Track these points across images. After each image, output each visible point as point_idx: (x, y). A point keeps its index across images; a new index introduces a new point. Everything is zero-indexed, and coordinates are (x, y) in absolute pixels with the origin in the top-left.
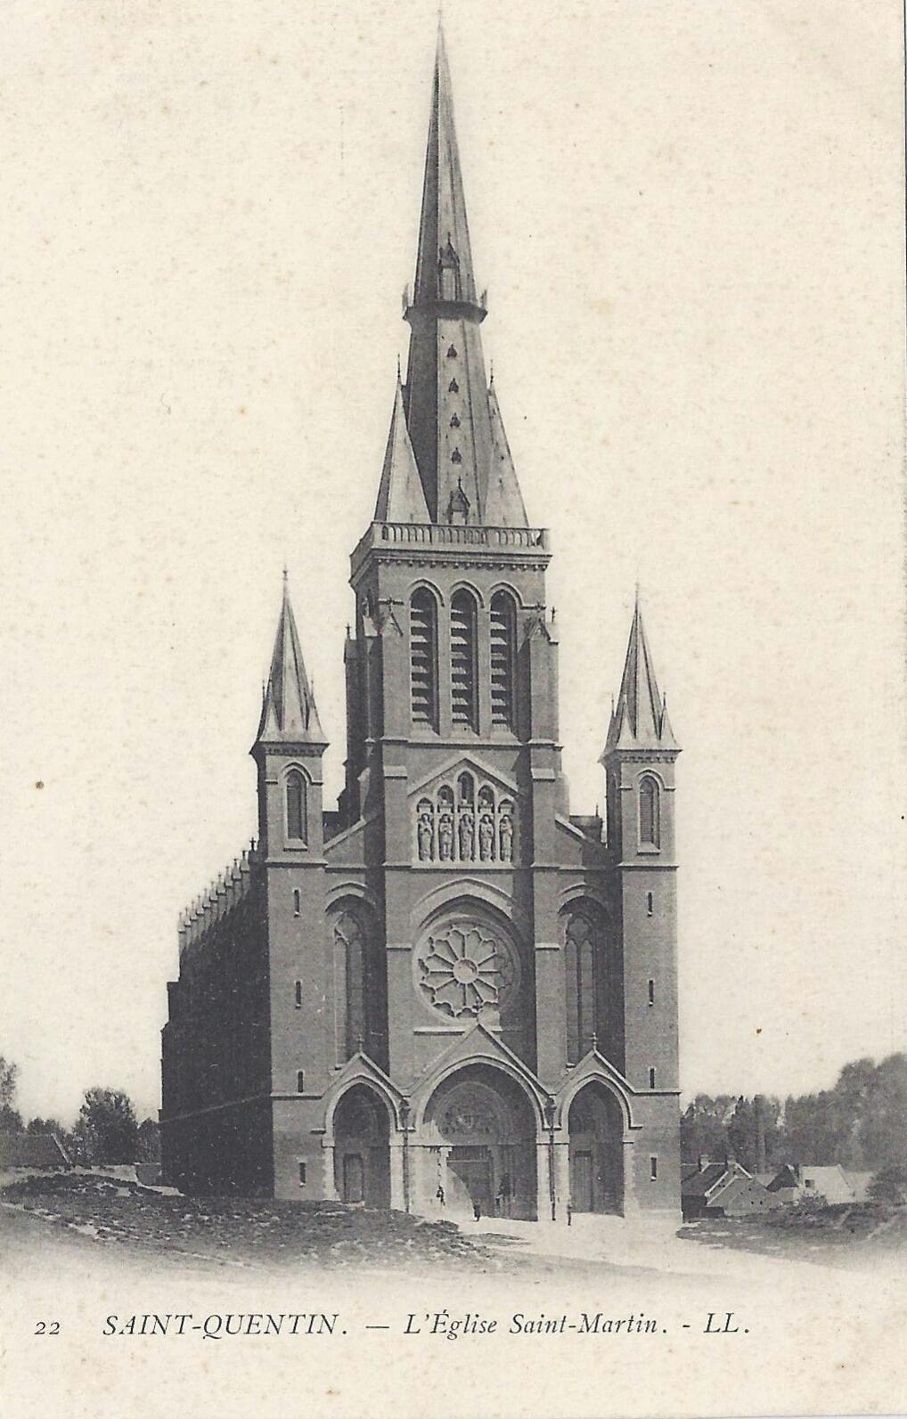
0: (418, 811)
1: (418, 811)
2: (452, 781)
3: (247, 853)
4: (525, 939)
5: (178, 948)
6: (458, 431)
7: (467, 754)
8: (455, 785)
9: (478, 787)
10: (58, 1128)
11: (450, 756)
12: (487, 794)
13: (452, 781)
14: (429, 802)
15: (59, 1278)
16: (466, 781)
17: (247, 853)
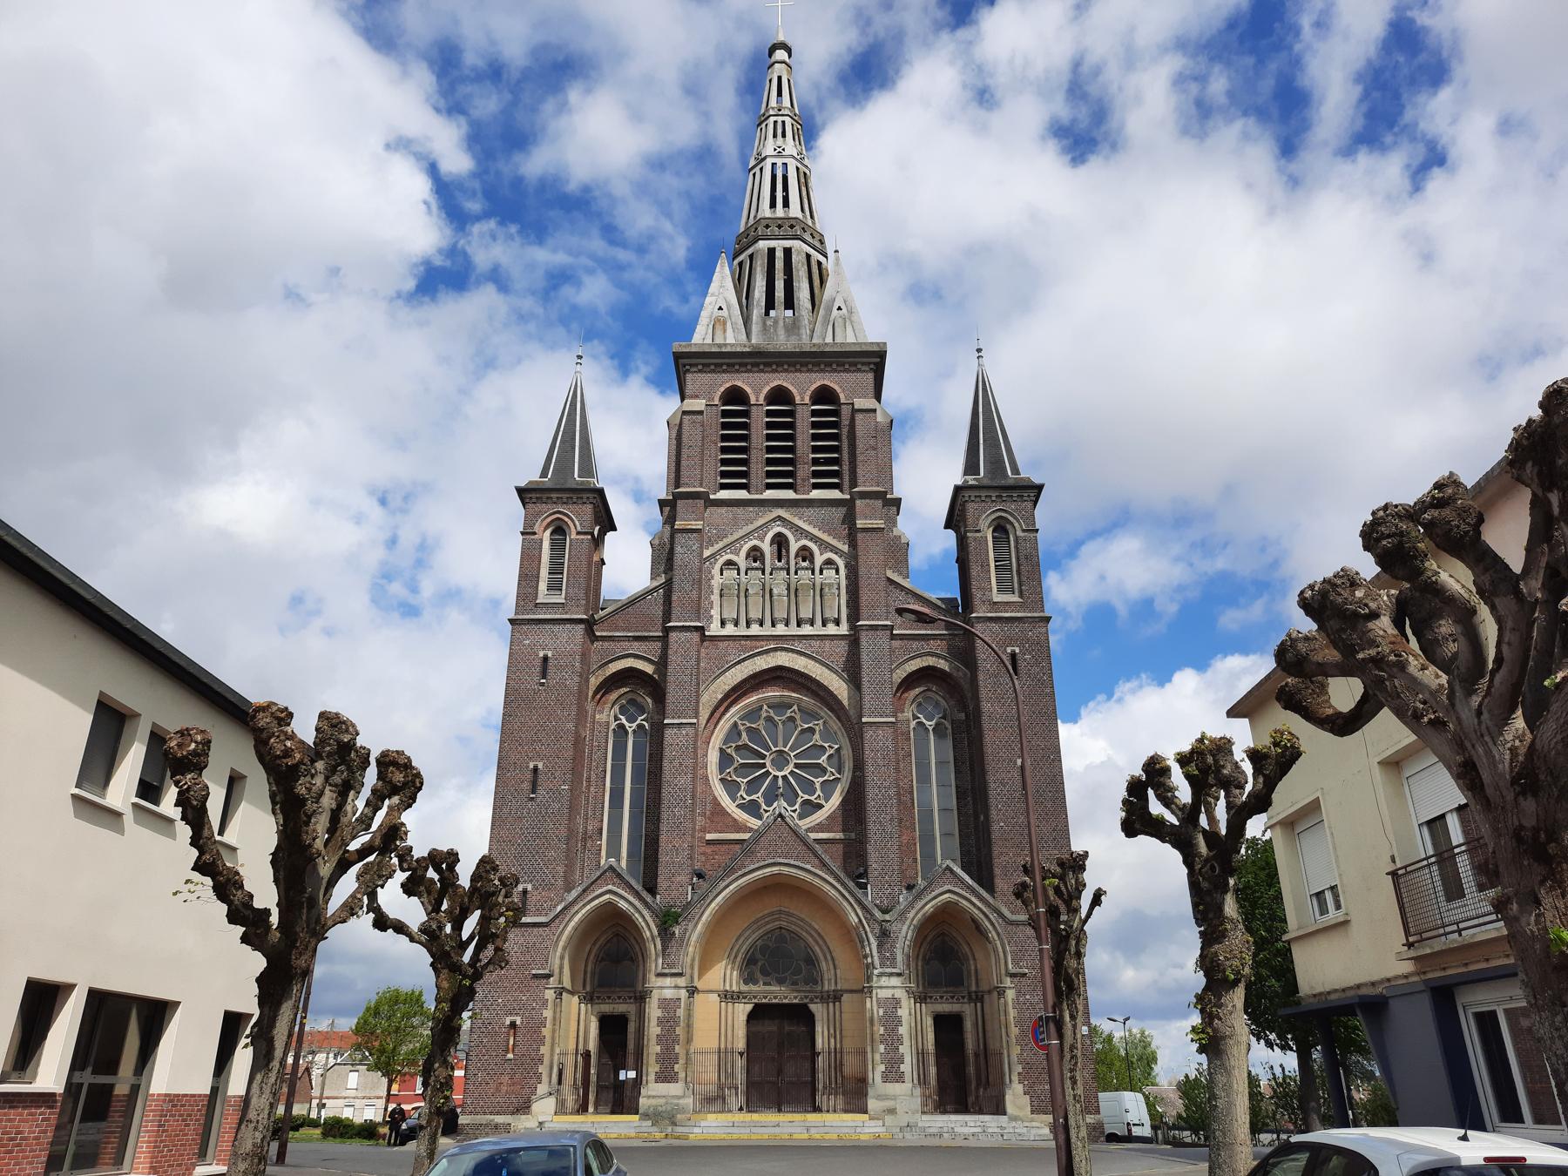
0: (722, 574)
1: (722, 574)
2: (738, 555)
3: (1453, 823)
4: (962, 632)
5: (41, 1070)
6: (499, 939)
7: (781, 512)
8: (766, 547)
9: (794, 546)
10: (319, 915)
11: (736, 524)
12: (805, 553)
13: (738, 555)
14: (735, 564)
15: (463, 741)
16: (780, 542)
17: (1453, 823)
